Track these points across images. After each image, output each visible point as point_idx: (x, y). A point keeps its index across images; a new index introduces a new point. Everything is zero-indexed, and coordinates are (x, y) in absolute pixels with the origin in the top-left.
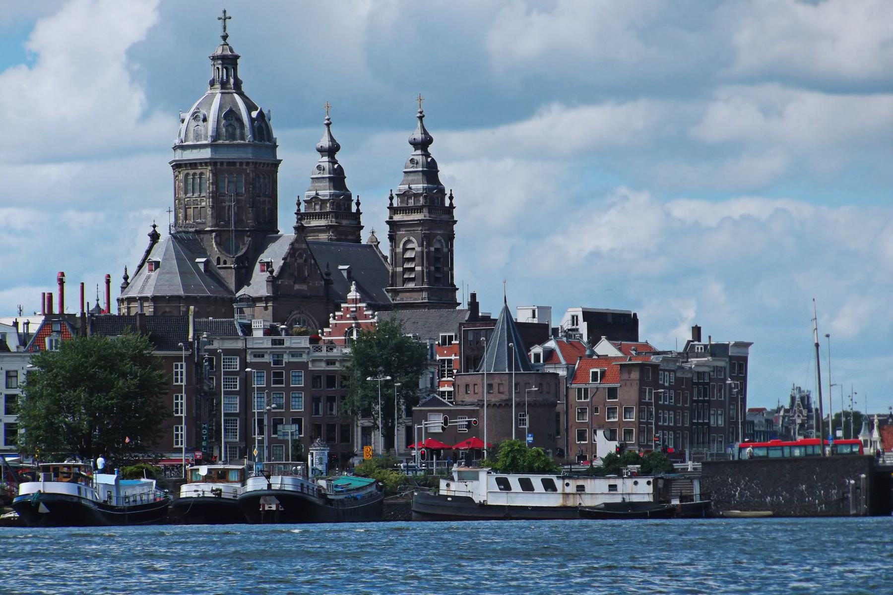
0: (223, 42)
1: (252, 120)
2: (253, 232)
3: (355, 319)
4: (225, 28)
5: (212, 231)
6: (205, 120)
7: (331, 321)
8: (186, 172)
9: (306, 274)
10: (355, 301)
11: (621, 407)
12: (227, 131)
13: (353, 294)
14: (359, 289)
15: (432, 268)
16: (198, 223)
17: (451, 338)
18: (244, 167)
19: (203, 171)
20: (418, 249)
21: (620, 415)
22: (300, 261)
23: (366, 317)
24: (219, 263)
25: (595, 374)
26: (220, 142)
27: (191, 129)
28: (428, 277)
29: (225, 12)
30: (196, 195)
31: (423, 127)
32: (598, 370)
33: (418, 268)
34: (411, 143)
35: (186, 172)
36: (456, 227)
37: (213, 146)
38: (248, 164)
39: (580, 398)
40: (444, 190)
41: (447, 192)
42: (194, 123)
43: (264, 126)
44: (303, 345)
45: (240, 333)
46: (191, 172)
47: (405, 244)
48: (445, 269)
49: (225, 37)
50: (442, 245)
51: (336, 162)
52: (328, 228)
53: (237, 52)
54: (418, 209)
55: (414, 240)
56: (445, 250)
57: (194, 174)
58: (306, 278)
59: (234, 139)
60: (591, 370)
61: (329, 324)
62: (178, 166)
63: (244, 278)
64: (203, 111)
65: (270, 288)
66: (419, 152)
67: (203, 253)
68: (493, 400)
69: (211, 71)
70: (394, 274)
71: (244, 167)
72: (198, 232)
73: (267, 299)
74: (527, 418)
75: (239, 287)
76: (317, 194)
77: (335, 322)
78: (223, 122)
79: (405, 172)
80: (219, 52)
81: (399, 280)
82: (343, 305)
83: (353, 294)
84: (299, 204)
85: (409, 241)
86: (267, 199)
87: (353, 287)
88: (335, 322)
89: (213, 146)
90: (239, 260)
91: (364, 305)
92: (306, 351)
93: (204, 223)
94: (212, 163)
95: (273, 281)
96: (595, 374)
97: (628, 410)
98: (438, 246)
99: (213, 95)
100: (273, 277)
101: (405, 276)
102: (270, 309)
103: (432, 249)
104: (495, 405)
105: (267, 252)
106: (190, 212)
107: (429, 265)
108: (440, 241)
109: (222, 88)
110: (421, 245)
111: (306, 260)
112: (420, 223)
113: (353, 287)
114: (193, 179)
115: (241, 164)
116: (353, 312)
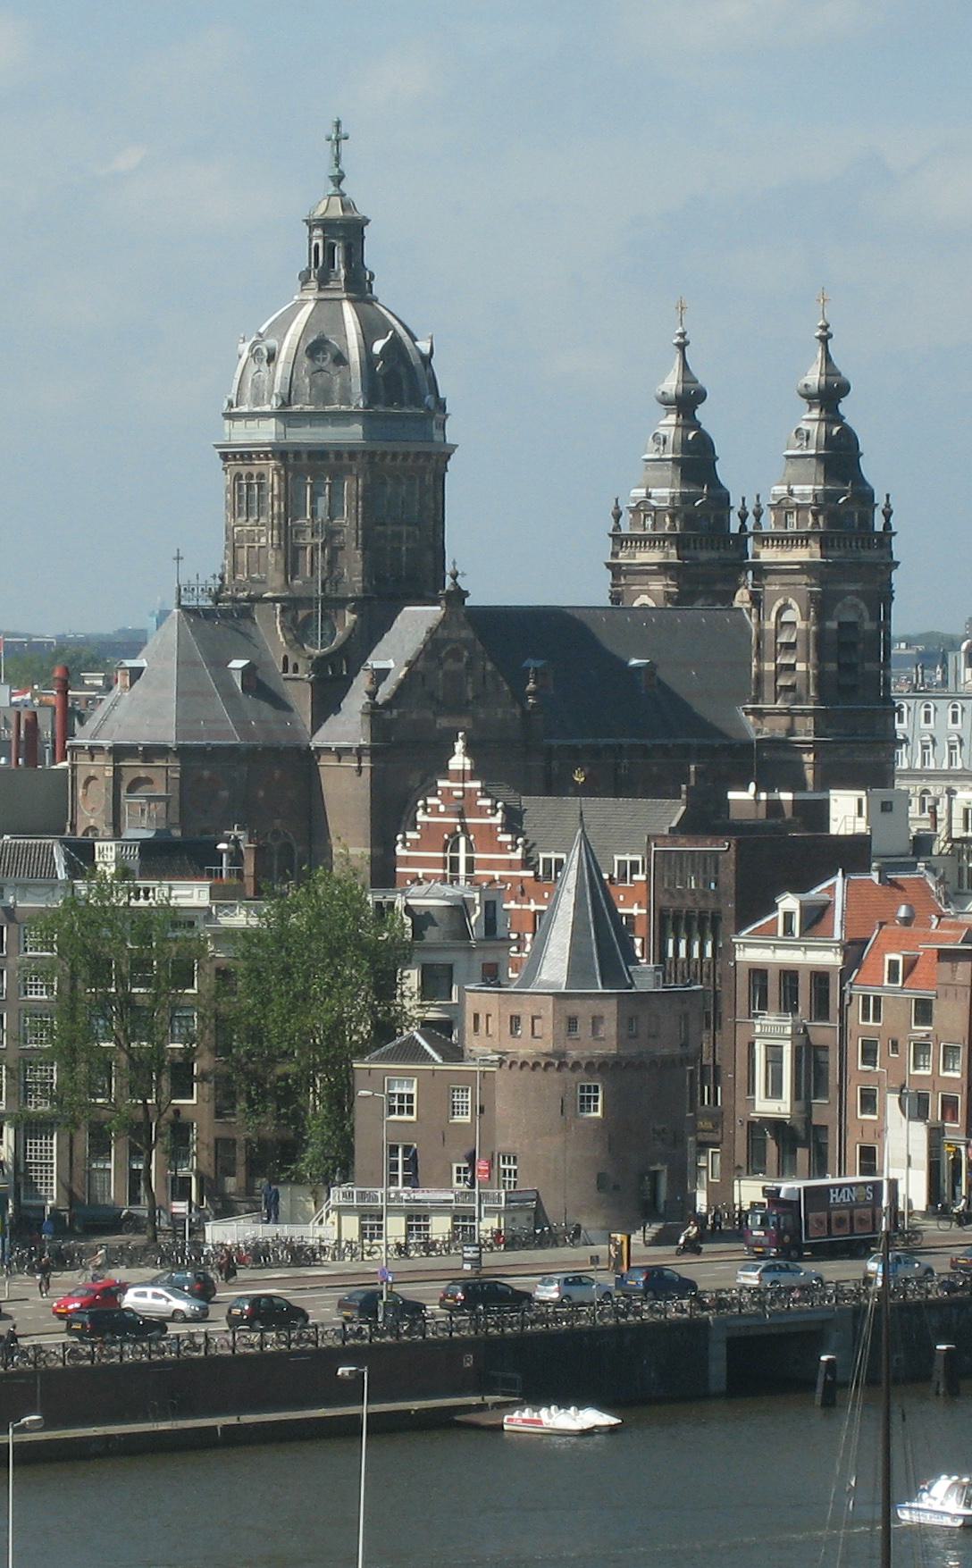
0: (332, 189)
1: (368, 359)
2: (360, 605)
3: (461, 815)
4: (338, 159)
5: (275, 600)
6: (272, 357)
7: (421, 817)
8: (237, 469)
9: (470, 695)
10: (462, 776)
11: (938, 1043)
12: (312, 383)
13: (459, 761)
14: (468, 752)
15: (832, 667)
16: (253, 580)
17: (634, 865)
18: (346, 461)
19: (263, 469)
20: (801, 625)
21: (936, 1061)
22: (450, 665)
23: (481, 812)
24: (285, 670)
25: (893, 964)
26: (296, 408)
27: (249, 377)
28: (818, 687)
29: (338, 124)
30: (252, 520)
31: (828, 358)
32: (900, 958)
33: (801, 667)
34: (803, 396)
35: (237, 469)
36: (896, 576)
37: (285, 415)
38: (352, 455)
39: (866, 1017)
40: (871, 494)
41: (880, 499)
42: (253, 368)
43: (402, 370)
44: (194, 902)
45: (62, 874)
46: (244, 470)
47: (779, 614)
48: (869, 666)
49: (338, 179)
50: (861, 616)
51: (697, 426)
52: (664, 568)
53: (362, 210)
54: (800, 539)
55: (795, 605)
56: (869, 626)
57: (250, 476)
58: (468, 703)
59: (328, 402)
60: (888, 957)
61: (415, 822)
62: (229, 456)
63: (327, 701)
64: (272, 342)
65: (367, 728)
66: (815, 414)
67: (248, 643)
68: (522, 1051)
69: (298, 249)
70: (760, 677)
71: (346, 461)
72: (249, 599)
73: (360, 752)
74: (600, 1094)
75: (318, 721)
76: (649, 496)
77: (426, 819)
78: (306, 362)
79: (788, 457)
80: (319, 213)
81: (768, 690)
82: (441, 783)
83: (459, 761)
84: (617, 516)
85: (785, 607)
86: (404, 529)
87: (459, 746)
88: (426, 819)
89: (285, 415)
90: (319, 664)
91: (477, 784)
92: (202, 915)
93: (263, 582)
94: (281, 452)
95: (375, 713)
96: (893, 964)
97: (950, 1052)
98: (850, 617)
99: (303, 302)
100: (375, 706)
101: (781, 682)
102: (366, 774)
103: (832, 625)
104: (524, 1064)
105: (381, 646)
106: (243, 554)
107: (821, 658)
108: (855, 606)
109: (320, 290)
110: (805, 617)
111: (470, 664)
112: (805, 568)
113: (459, 746)
114: (249, 486)
115: (339, 455)
116: (457, 798)
